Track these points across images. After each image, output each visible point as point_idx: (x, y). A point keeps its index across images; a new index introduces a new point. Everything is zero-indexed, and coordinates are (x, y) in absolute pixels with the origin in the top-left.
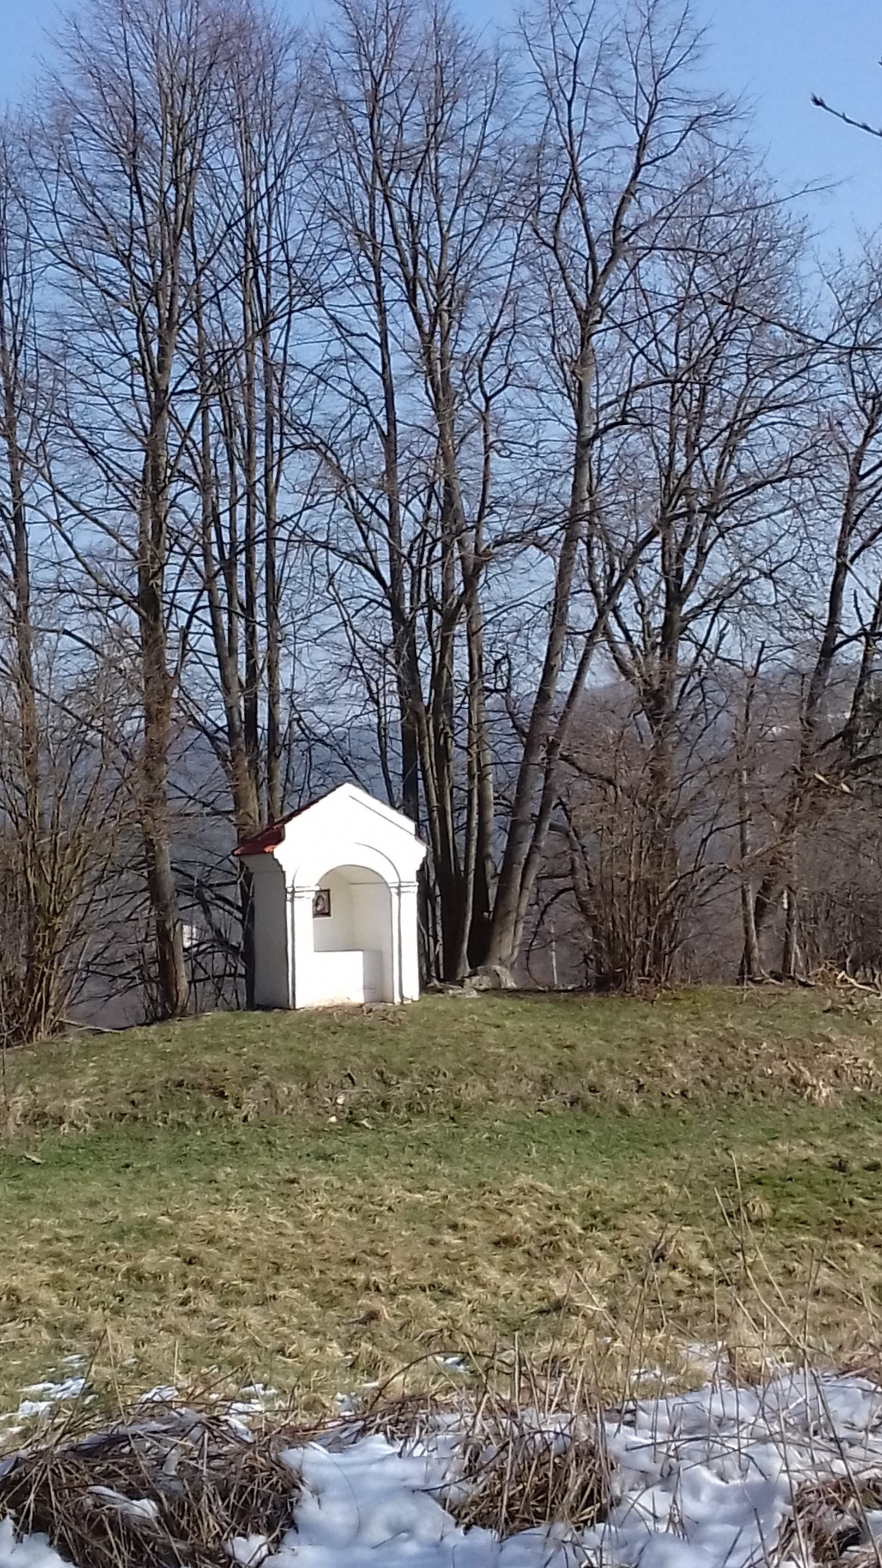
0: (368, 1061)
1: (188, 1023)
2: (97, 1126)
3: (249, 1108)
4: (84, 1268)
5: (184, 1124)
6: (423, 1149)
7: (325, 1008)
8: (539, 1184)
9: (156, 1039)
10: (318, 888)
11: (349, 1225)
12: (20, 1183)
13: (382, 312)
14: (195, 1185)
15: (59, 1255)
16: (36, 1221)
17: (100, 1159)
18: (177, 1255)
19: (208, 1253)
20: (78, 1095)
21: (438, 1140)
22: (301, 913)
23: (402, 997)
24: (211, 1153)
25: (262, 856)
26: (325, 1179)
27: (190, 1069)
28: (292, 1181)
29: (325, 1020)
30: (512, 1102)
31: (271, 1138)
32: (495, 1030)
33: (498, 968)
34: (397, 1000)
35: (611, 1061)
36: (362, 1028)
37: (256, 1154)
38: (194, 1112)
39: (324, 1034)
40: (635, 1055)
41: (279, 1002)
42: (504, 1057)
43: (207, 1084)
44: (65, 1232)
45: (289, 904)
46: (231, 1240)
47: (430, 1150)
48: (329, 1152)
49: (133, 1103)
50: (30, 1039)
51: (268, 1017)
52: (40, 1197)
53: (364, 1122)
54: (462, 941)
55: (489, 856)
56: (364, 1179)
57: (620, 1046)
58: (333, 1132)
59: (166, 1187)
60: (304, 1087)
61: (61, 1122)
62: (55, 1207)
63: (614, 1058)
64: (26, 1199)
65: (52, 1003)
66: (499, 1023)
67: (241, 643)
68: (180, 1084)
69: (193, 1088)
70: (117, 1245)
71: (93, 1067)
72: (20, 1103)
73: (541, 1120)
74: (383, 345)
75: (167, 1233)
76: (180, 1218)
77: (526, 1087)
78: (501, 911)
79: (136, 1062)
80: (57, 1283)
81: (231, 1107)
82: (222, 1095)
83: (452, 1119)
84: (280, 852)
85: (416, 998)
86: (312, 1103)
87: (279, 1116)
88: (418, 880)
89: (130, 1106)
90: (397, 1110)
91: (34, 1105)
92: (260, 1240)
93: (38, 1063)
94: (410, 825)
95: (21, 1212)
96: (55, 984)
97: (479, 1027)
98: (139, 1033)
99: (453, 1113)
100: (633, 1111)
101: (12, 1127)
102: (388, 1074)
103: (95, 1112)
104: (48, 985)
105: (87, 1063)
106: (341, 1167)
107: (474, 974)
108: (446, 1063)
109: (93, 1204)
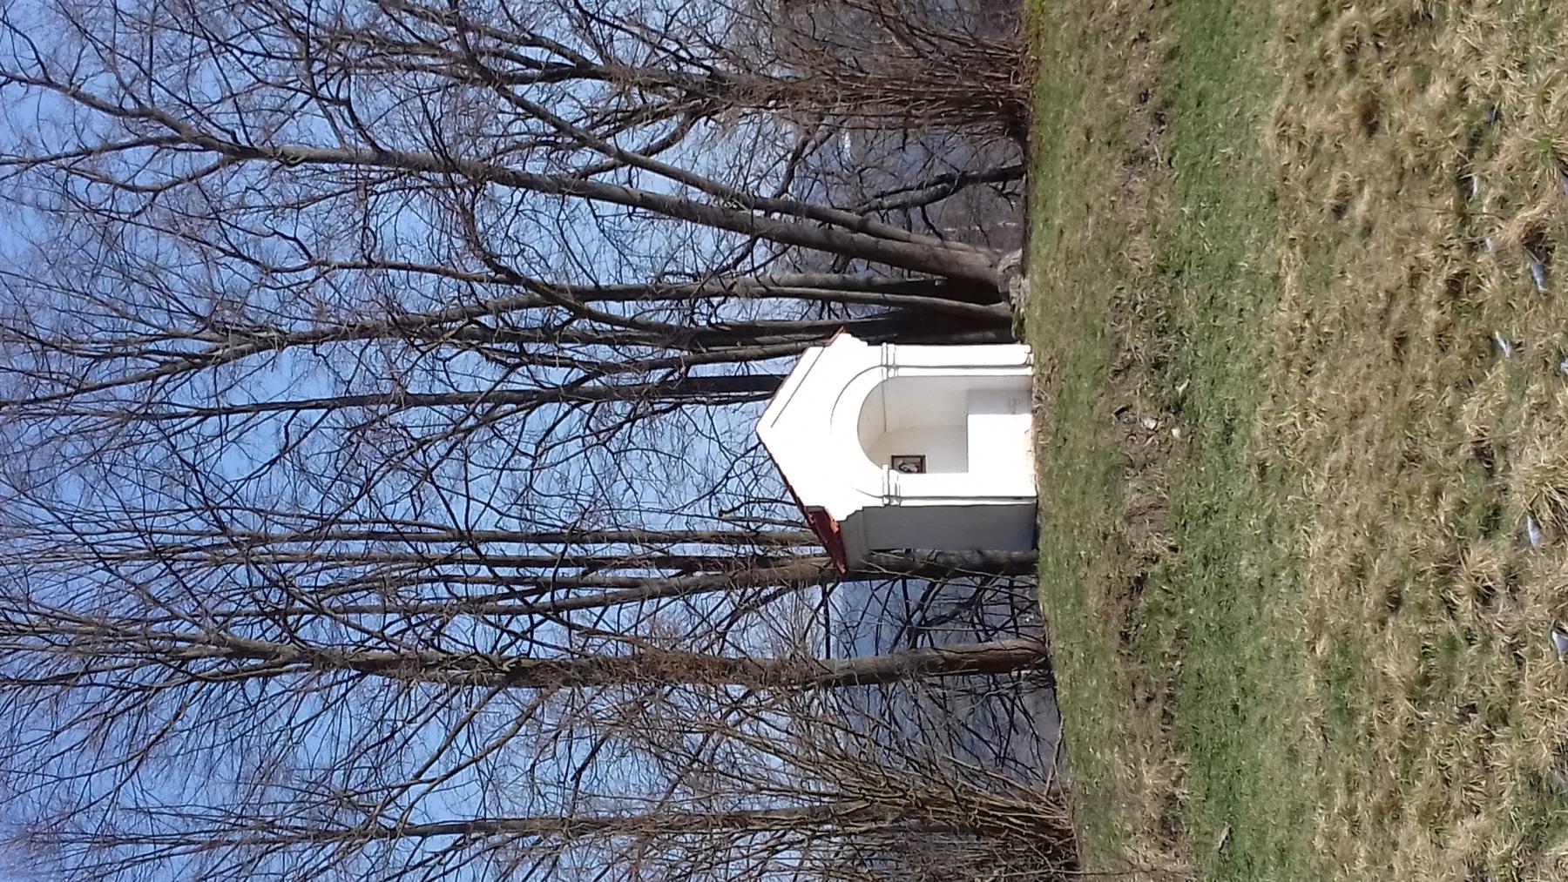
0: (1100, 390)
1: (1052, 632)
2: (1179, 748)
3: (1159, 545)
4: (1406, 772)
5: (1178, 632)
6: (1219, 302)
7: (1039, 460)
8: (1273, 114)
9: (1070, 672)
10: (886, 467)
11: (1333, 370)
12: (1258, 861)
13: (260, 407)
14: (1266, 609)
15: (1380, 812)
16: (1319, 843)
17: (1224, 746)
18: (1383, 623)
19: (1382, 573)
20: (1138, 774)
21: (1207, 284)
22: (915, 488)
23: (1025, 365)
24: (1220, 593)
25: (845, 535)
26: (1260, 423)
27: (1106, 622)
28: (1263, 468)
29: (1049, 456)
30: (1157, 200)
31: (1200, 511)
32: (1066, 235)
33: (1001, 268)
34: (1029, 371)
35: (1108, 79)
36: (1061, 403)
37: (1221, 530)
38: (1162, 618)
39: (1065, 453)
40: (1101, 50)
41: (1026, 519)
42: (1099, 216)
43: (1125, 601)
44: (1340, 799)
45: (905, 503)
46: (1358, 541)
47: (1220, 292)
48: (1220, 428)
49: (1148, 700)
50: (1064, 833)
51: (1046, 527)
52: (1281, 833)
53: (1180, 389)
54: (968, 310)
55: (869, 280)
56: (1259, 368)
57: (1089, 73)
58: (1193, 433)
59: (1268, 650)
60: (1132, 472)
61: (1172, 797)
62: (1297, 813)
63: (1103, 74)
64: (1283, 854)
65: (1023, 804)
66: (1056, 232)
67: (631, 573)
68: (1125, 636)
69: (1129, 619)
70: (1363, 719)
71: (1102, 755)
72: (1144, 852)
73: (1184, 158)
74: (297, 407)
75: (1344, 642)
76: (1319, 625)
77: (1139, 185)
78: (935, 265)
79: (1096, 697)
80: (1435, 818)
81: (1157, 568)
82: (1141, 581)
83: (1178, 273)
84: (838, 513)
85: (1027, 348)
86: (1154, 461)
87: (1171, 502)
88: (880, 343)
89: (1154, 704)
90: (1166, 348)
91: (1149, 834)
92: (1361, 497)
93: (1096, 825)
94: (812, 352)
95: (1303, 863)
96: (999, 801)
97: (1061, 256)
98: (1063, 693)
99: (1171, 274)
100: (1174, 42)
101: (1179, 866)
102: (1117, 364)
103: (1160, 752)
104: (1002, 809)
105: (1098, 762)
106: (1243, 406)
107: (1007, 297)
108: (1104, 288)
109: (1293, 756)
